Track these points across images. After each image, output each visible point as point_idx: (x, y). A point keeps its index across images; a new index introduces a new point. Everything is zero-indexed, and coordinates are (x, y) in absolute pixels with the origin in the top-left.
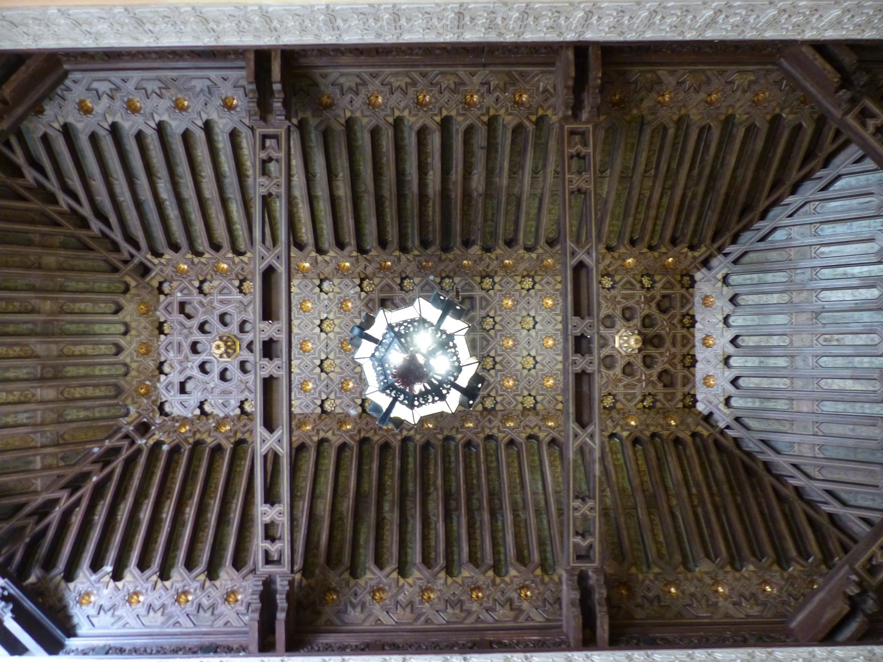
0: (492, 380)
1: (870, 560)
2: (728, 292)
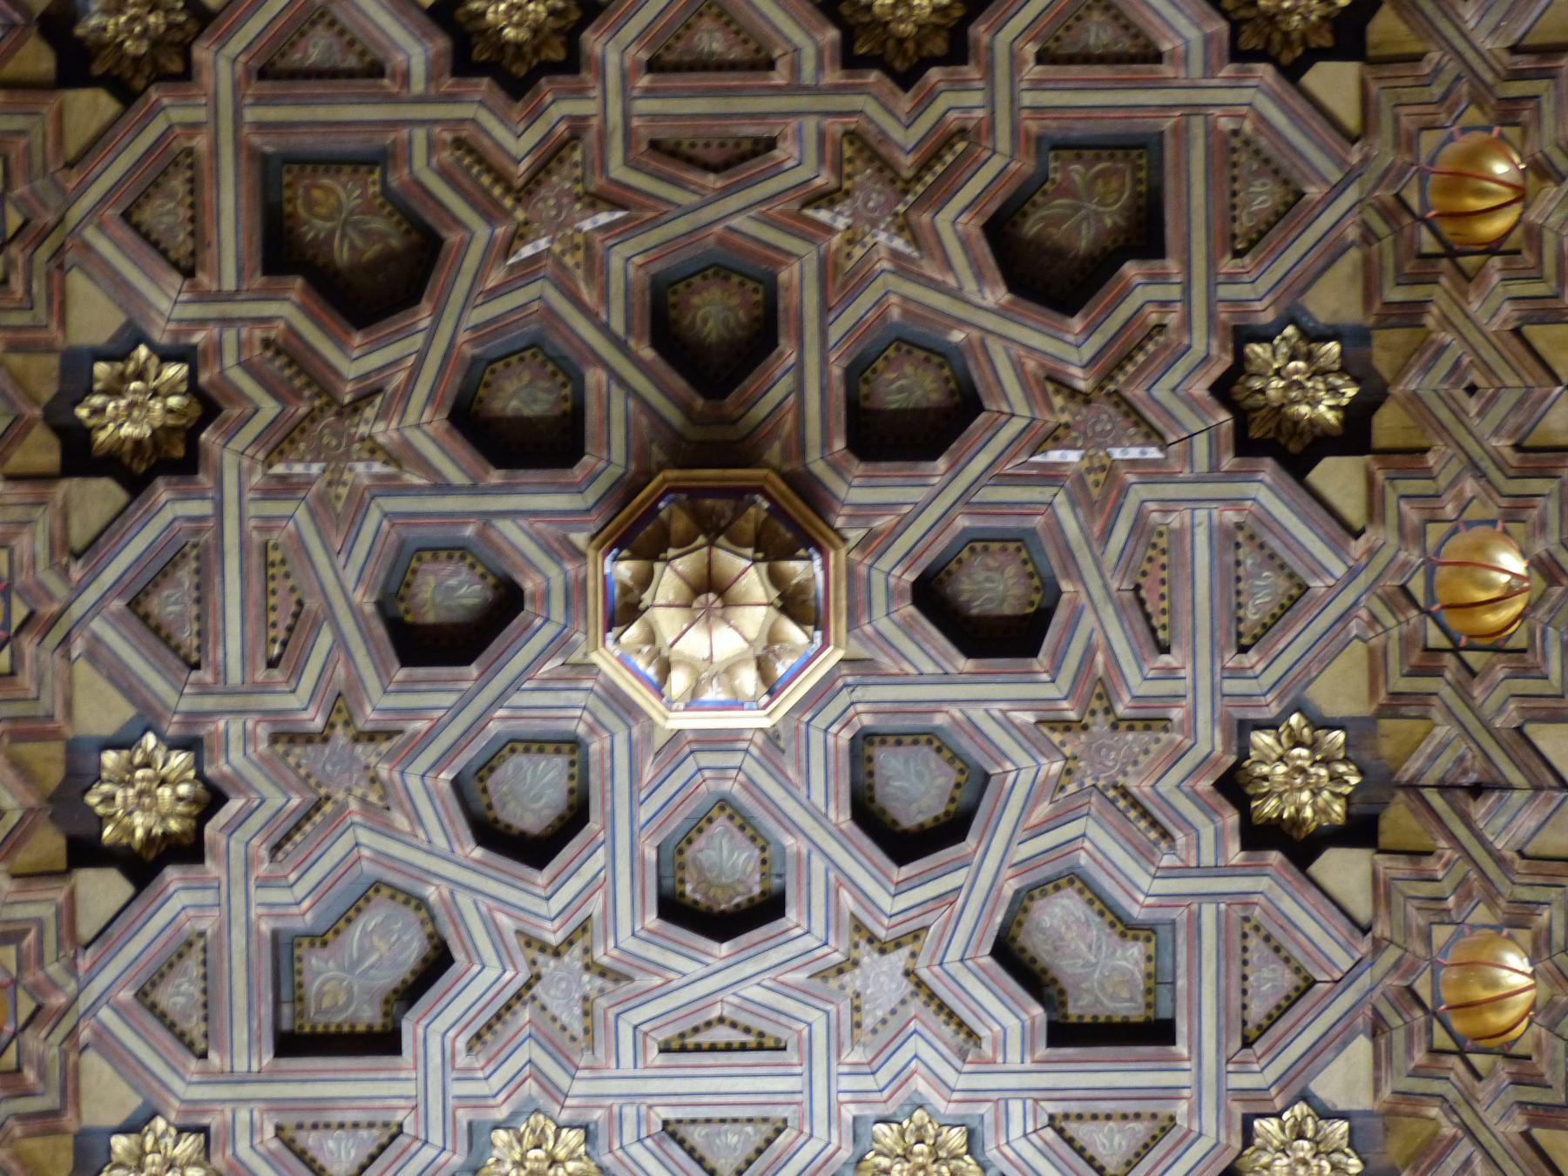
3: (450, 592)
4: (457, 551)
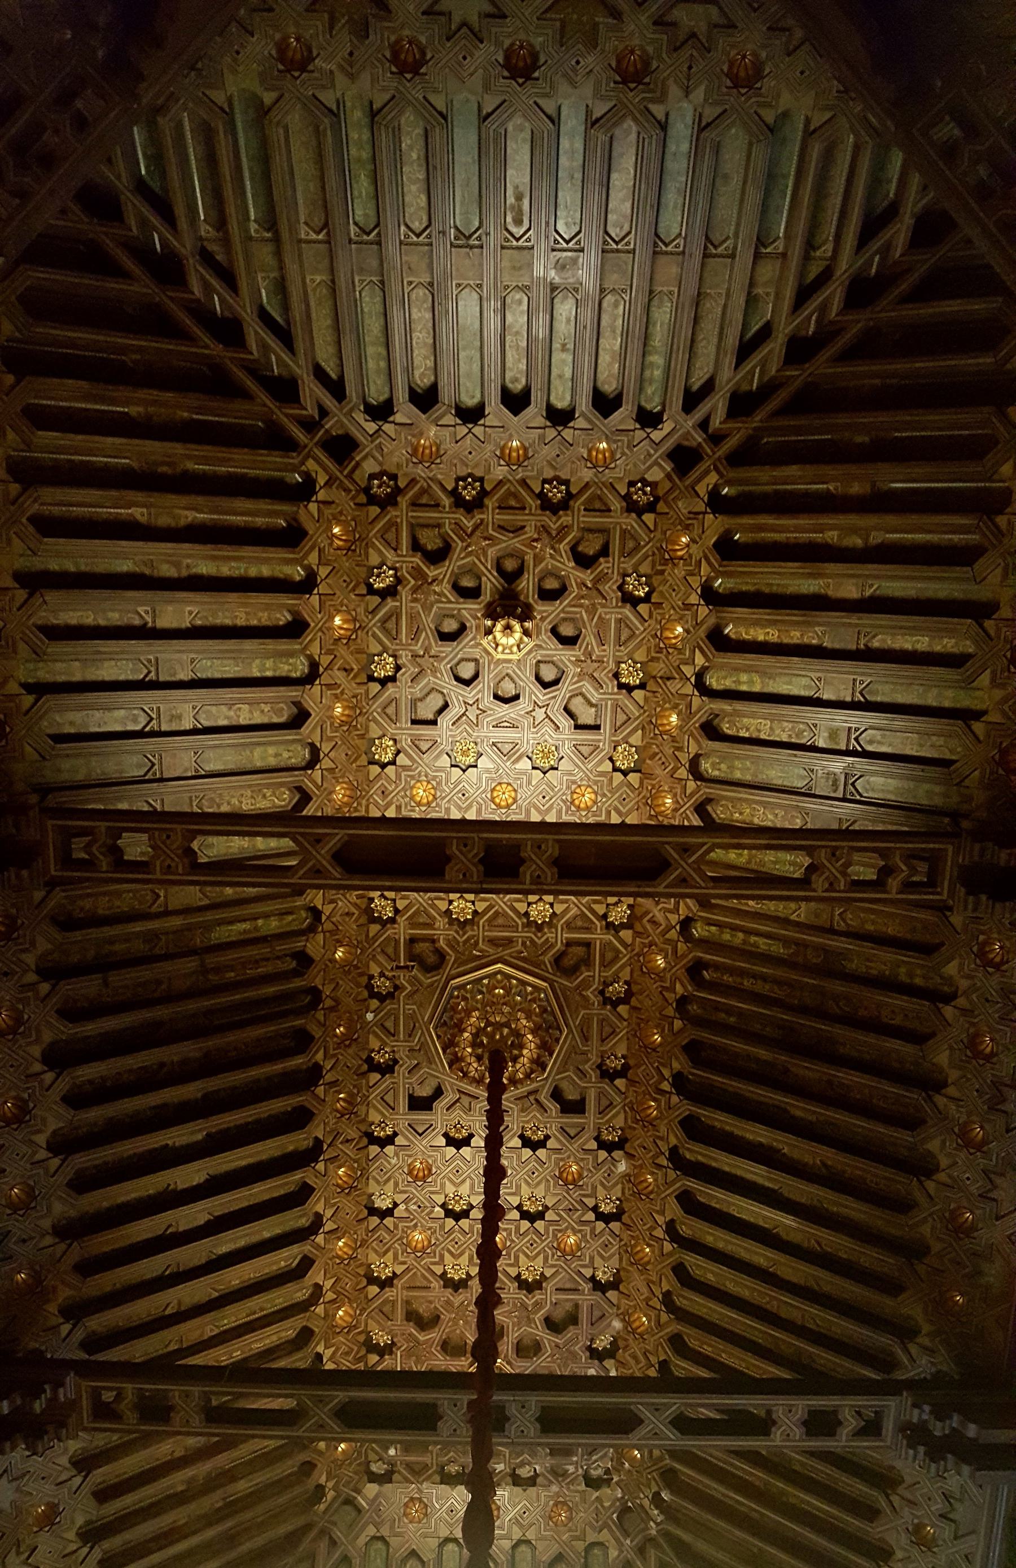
0: (574, 911)
2: (405, 412)
3: (450, 626)
4: (453, 616)
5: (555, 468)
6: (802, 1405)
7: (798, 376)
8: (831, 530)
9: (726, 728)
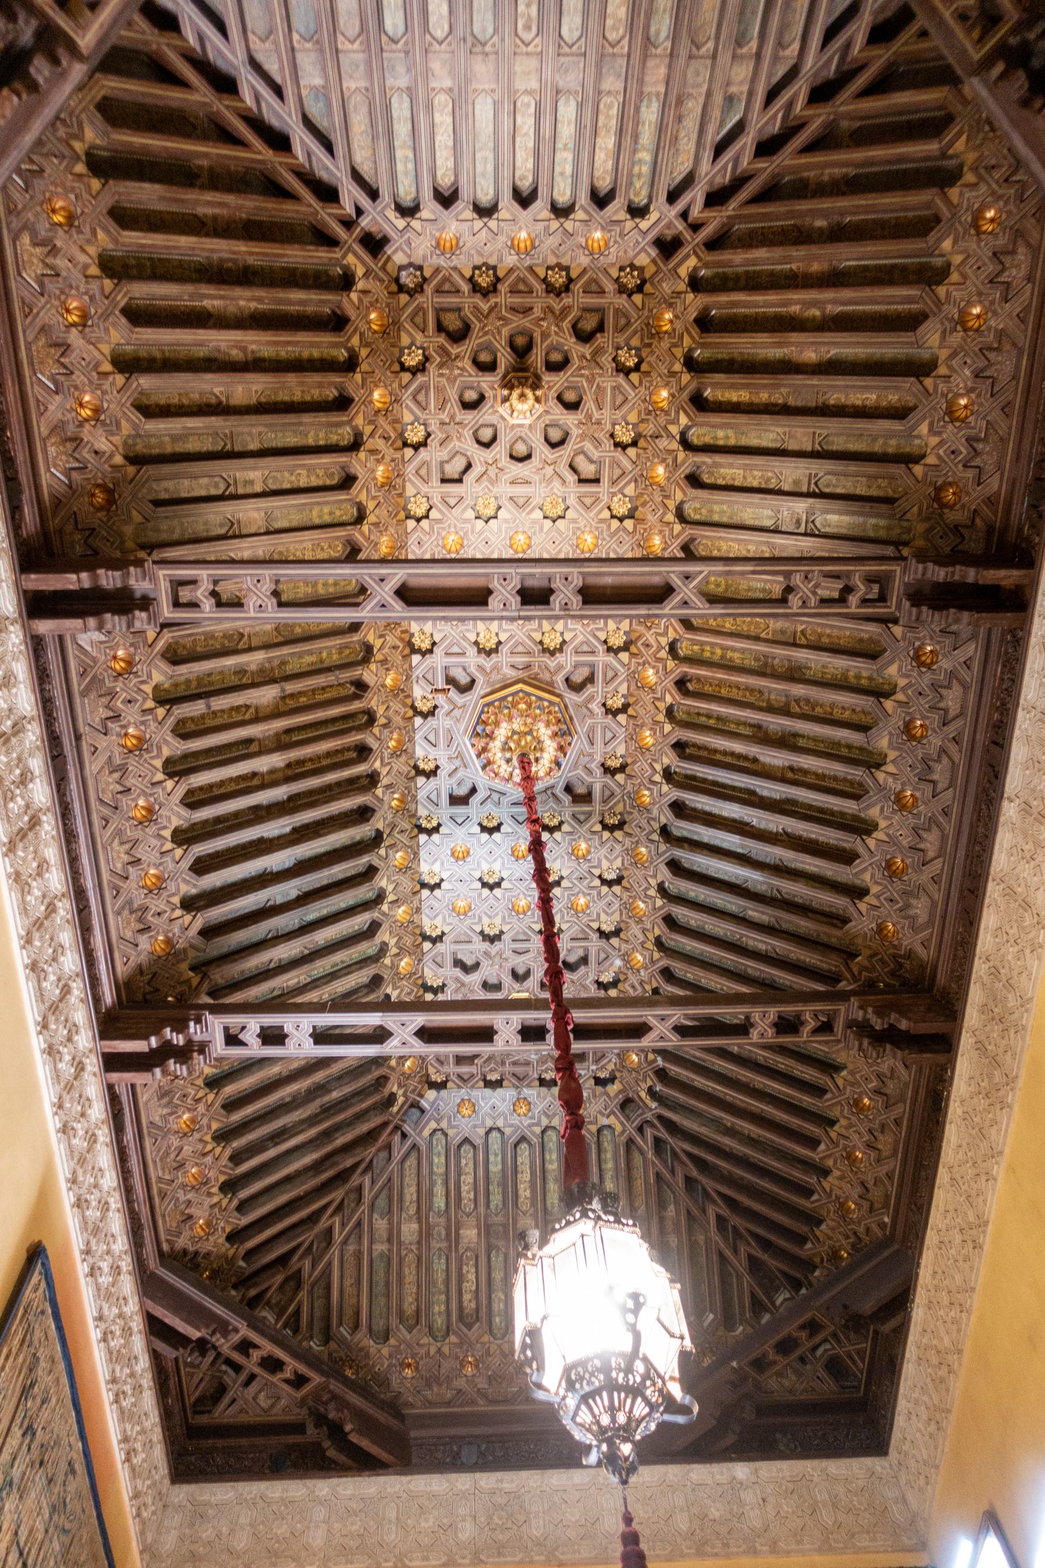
0: (581, 638)
1: (962, 17)
2: (430, 209)
3: (471, 396)
4: (472, 388)
5: (557, 256)
6: (772, 1012)
7: (767, 167)
8: (795, 302)
9: (706, 478)
